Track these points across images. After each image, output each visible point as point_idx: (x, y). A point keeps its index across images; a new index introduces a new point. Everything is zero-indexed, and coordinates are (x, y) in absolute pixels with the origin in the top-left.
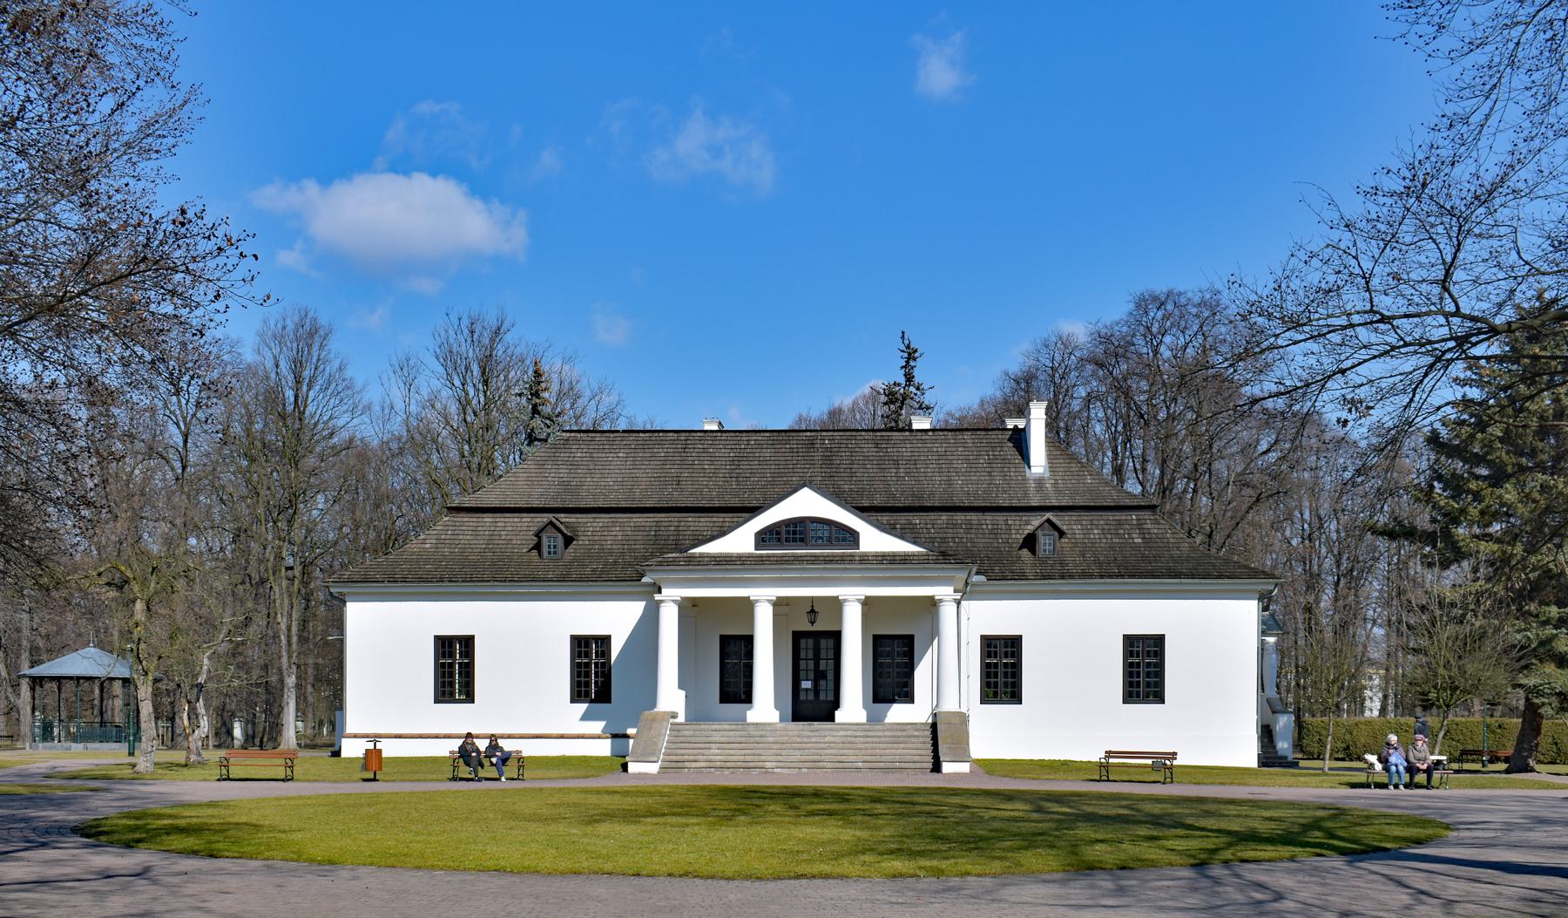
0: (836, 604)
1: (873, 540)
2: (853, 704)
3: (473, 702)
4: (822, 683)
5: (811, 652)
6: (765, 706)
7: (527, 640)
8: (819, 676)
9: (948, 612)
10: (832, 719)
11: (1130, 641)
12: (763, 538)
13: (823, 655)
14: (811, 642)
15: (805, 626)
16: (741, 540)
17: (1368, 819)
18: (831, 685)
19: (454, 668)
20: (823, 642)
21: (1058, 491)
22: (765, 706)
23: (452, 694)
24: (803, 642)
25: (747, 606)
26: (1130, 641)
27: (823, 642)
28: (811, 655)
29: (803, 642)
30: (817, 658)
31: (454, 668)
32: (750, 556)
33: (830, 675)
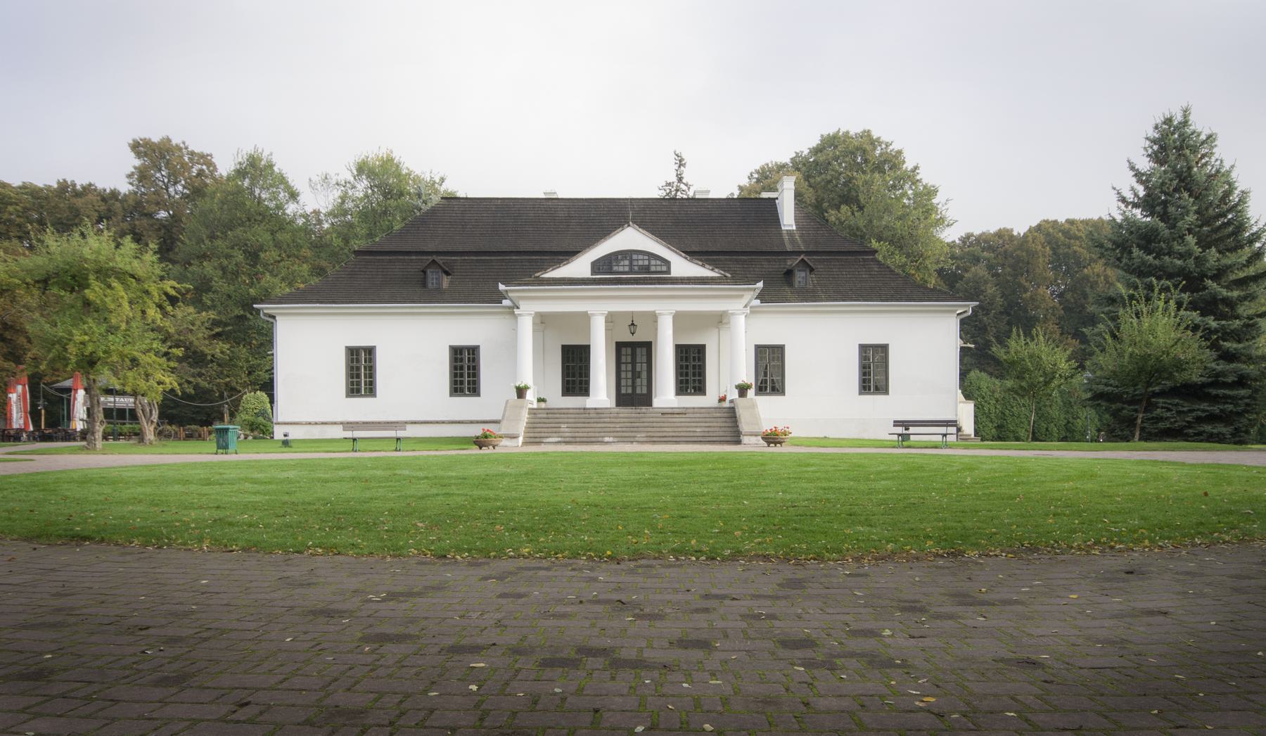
0: (653, 318)
1: (682, 266)
2: (666, 393)
3: (375, 396)
4: (638, 380)
5: (633, 356)
6: (602, 390)
7: (410, 343)
8: (636, 375)
9: (740, 322)
10: (650, 404)
11: (864, 348)
12: (597, 266)
13: (638, 360)
14: (629, 350)
15: (628, 338)
16: (580, 267)
17: (156, 537)
18: (645, 382)
19: (361, 371)
20: (638, 350)
21: (804, 241)
22: (602, 390)
23: (358, 391)
24: (624, 350)
25: (585, 318)
26: (864, 348)
27: (638, 350)
28: (629, 360)
29: (624, 350)
30: (634, 363)
31: (361, 371)
32: (588, 279)
33: (644, 375)
